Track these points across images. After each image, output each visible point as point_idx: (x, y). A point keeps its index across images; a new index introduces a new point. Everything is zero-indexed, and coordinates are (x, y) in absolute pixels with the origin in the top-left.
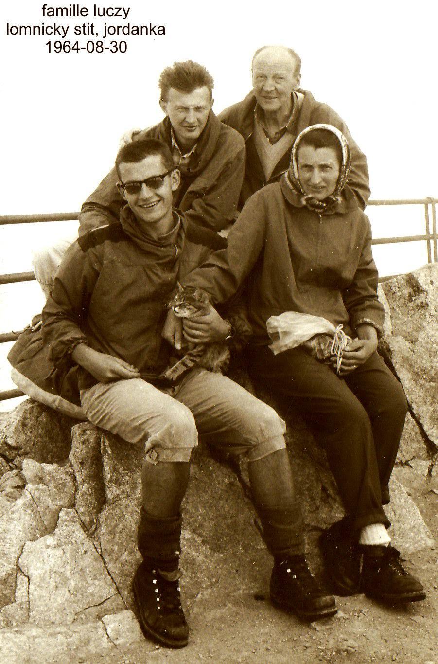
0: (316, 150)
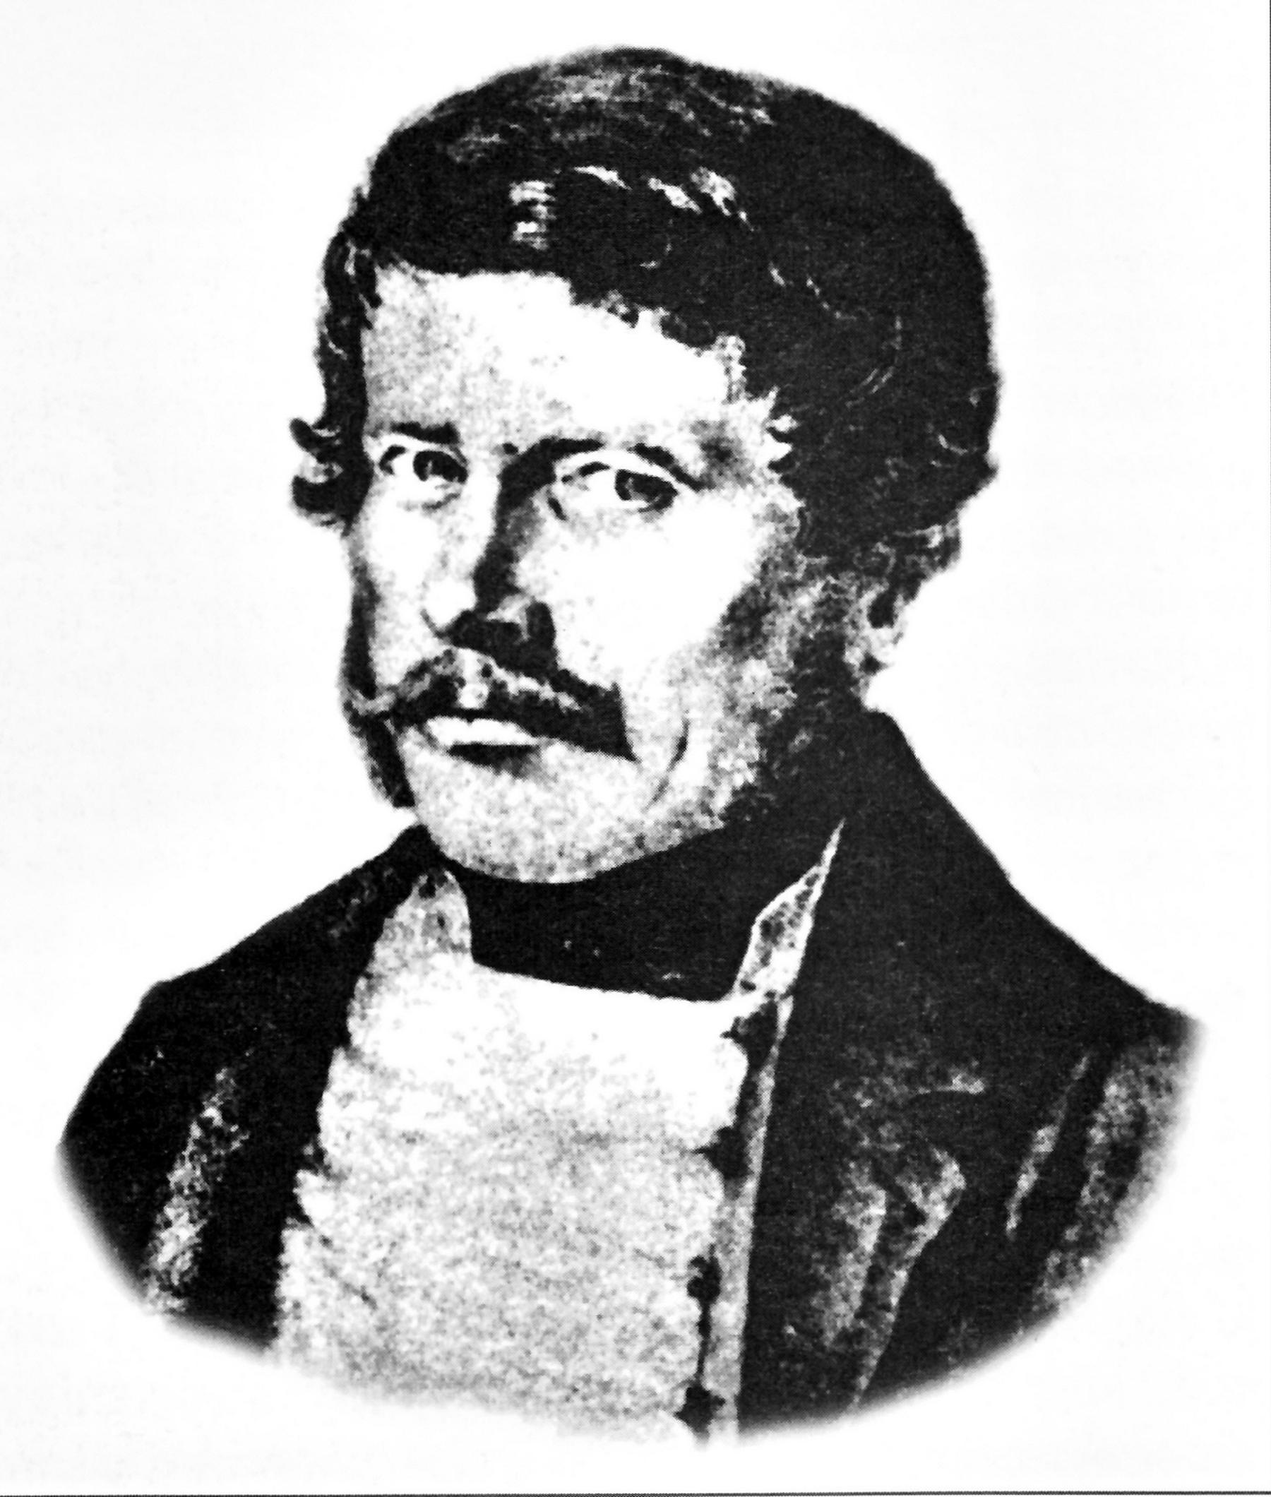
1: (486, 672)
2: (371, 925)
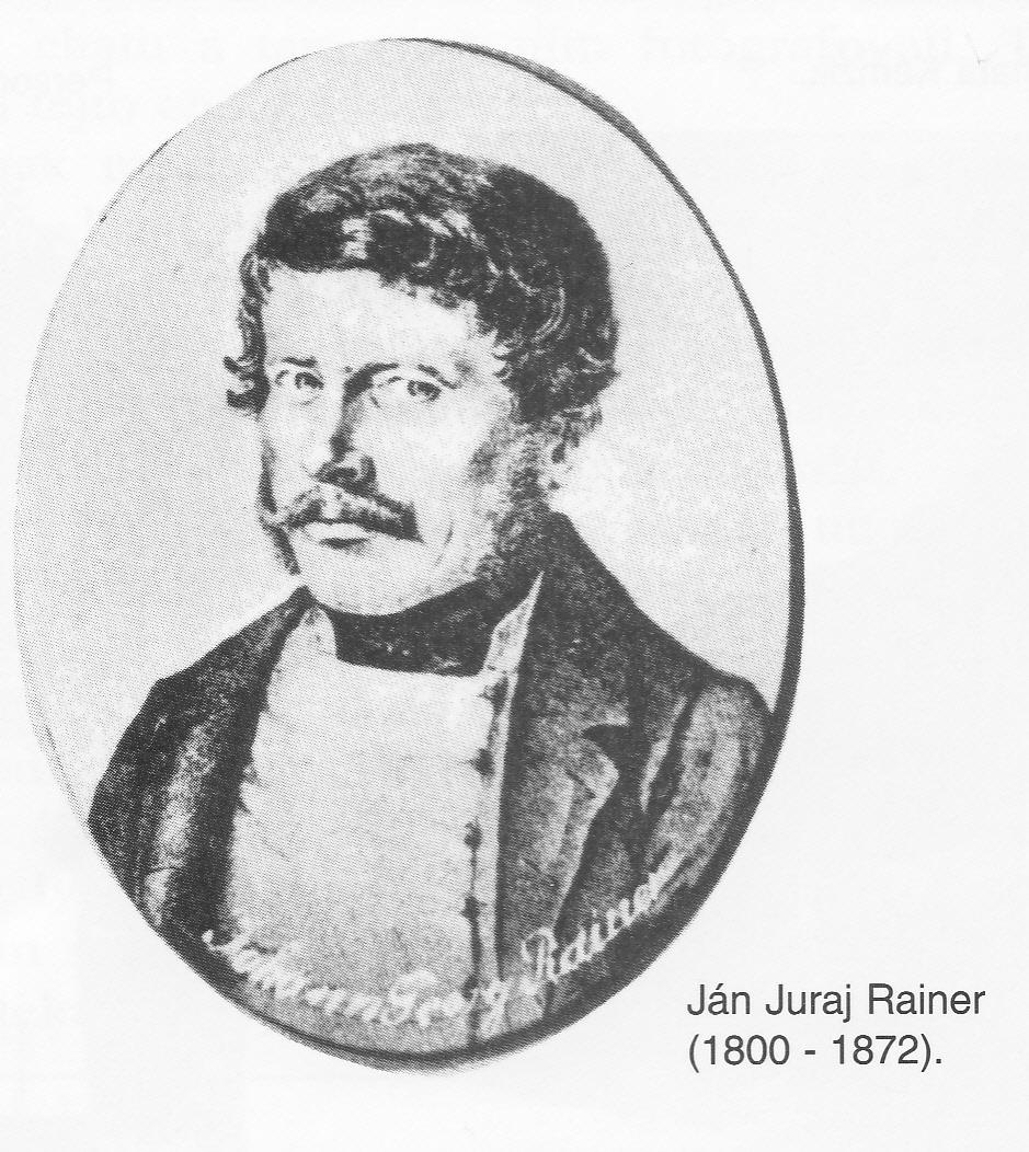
0: (618, 374)
1: (339, 497)
2: (279, 641)
